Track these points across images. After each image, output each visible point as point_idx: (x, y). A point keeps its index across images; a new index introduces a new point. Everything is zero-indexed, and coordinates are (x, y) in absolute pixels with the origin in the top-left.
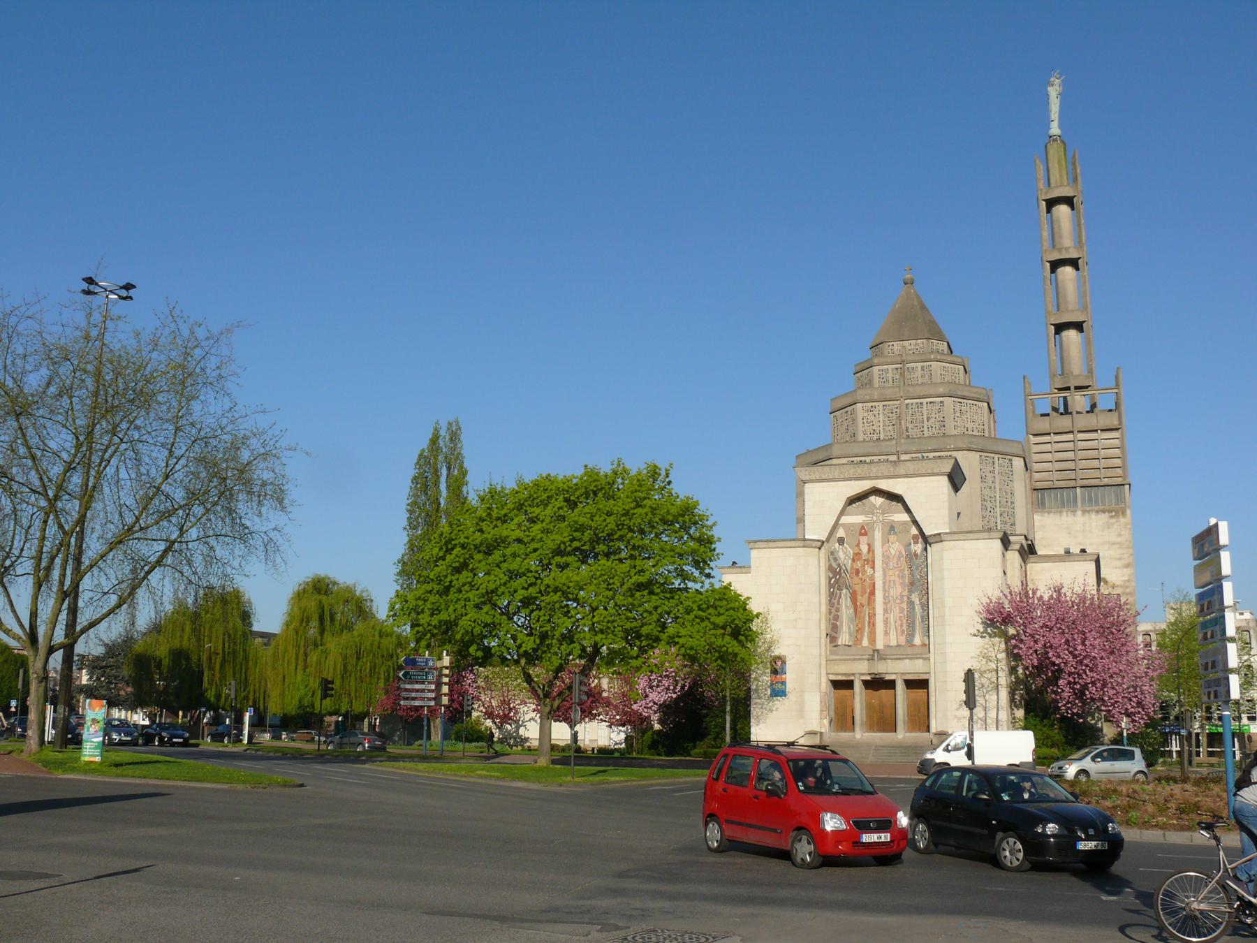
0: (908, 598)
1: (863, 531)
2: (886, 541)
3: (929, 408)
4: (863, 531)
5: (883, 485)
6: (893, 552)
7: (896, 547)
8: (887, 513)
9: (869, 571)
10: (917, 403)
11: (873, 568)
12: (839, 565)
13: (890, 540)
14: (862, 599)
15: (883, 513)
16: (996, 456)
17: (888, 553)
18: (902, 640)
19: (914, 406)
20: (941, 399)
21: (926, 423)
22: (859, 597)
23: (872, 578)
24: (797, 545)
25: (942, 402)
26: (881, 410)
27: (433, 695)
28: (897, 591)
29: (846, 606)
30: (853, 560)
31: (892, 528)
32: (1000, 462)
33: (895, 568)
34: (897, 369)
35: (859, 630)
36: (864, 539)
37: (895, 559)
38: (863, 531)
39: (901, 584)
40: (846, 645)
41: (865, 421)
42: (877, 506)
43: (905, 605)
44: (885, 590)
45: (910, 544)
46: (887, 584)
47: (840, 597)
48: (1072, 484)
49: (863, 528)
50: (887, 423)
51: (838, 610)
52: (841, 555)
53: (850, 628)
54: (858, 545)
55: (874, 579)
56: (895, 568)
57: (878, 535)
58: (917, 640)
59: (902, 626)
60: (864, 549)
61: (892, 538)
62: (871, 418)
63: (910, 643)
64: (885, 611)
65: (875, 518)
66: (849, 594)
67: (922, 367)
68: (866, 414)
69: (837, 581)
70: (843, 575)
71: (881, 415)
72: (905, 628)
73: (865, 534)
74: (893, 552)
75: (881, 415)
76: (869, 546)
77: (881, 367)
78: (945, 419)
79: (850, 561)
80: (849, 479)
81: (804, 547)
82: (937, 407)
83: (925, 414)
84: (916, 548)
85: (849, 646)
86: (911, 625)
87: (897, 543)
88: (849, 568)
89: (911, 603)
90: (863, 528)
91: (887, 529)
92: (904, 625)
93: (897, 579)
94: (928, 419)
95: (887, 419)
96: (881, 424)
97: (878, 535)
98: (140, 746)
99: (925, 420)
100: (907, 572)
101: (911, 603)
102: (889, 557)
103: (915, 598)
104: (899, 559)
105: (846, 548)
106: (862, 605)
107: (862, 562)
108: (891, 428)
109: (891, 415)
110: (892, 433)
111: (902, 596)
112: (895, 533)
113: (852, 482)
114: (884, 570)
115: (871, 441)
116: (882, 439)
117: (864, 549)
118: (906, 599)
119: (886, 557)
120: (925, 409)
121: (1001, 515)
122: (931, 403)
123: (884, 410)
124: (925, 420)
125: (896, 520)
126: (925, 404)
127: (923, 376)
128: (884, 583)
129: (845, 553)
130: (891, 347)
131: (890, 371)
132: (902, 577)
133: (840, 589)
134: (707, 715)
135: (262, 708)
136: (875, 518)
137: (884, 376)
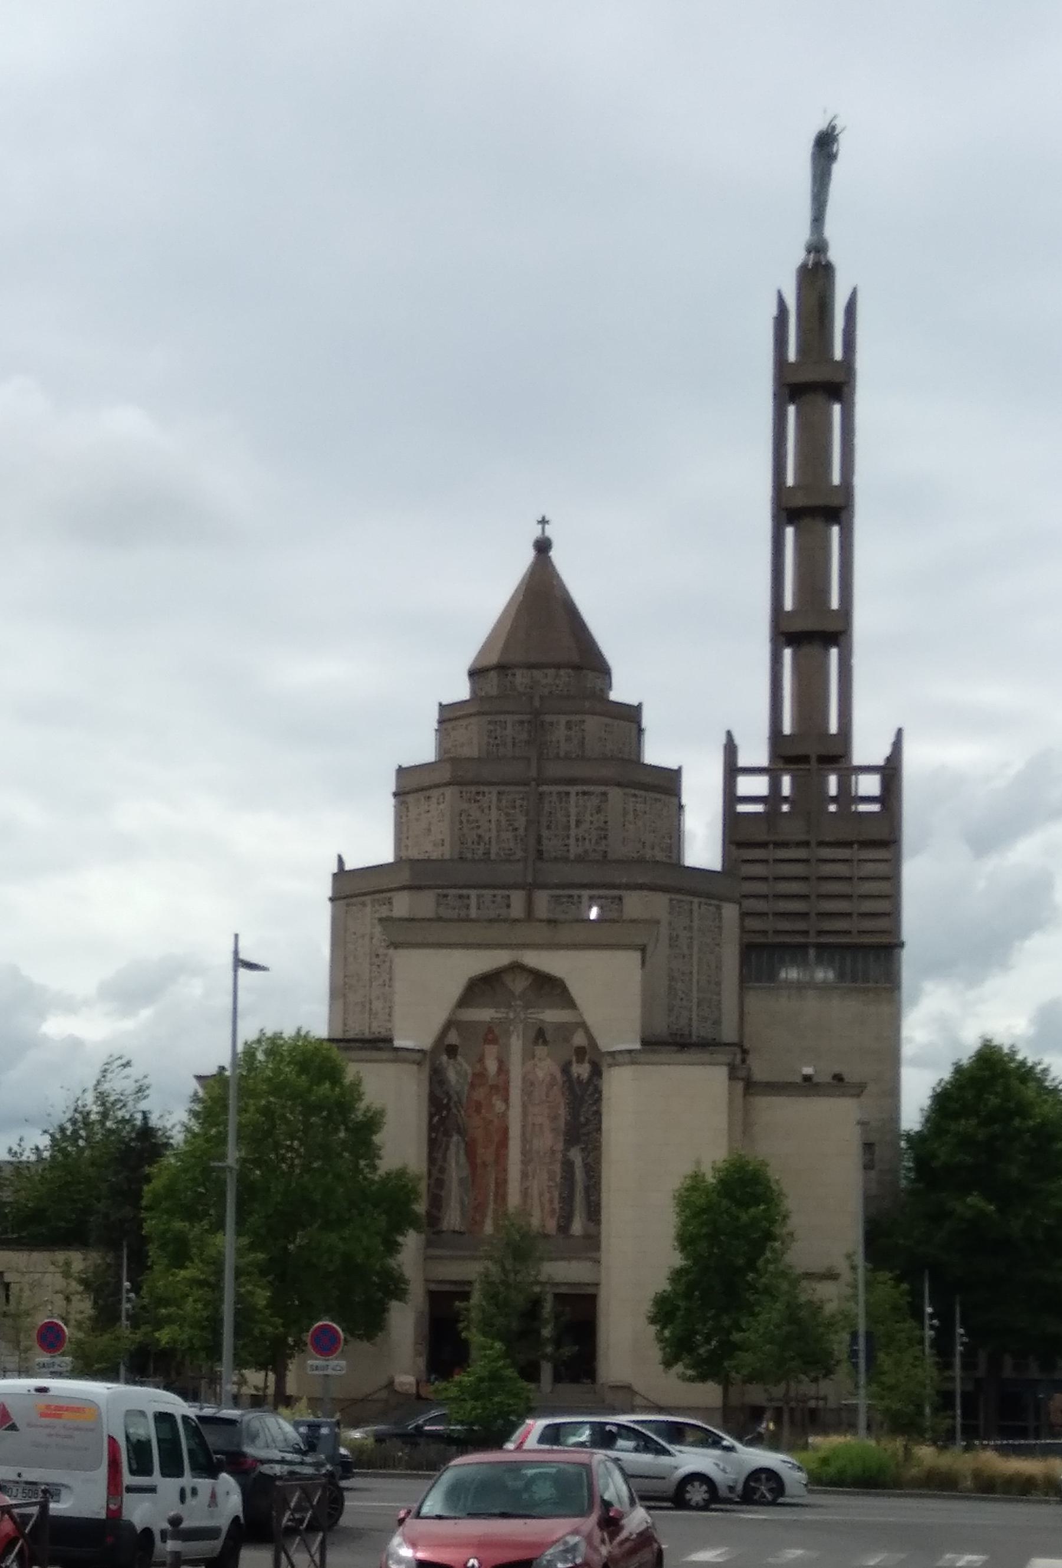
0: (564, 1156)
2: (528, 1055)
3: (581, 802)
4: (490, 1037)
5: (533, 959)
7: (546, 1067)
9: (499, 1105)
10: (559, 793)
11: (506, 1100)
12: (447, 1093)
14: (485, 1154)
15: (527, 1007)
16: (696, 900)
18: (551, 1226)
19: (554, 798)
20: (603, 789)
21: (573, 832)
22: (480, 1151)
23: (504, 1116)
25: (604, 794)
28: (547, 1141)
29: (457, 1163)
30: (472, 1085)
32: (703, 907)
34: (522, 722)
35: (480, 1208)
38: (491, 1034)
39: (553, 1130)
40: (454, 1232)
41: (464, 818)
42: (517, 994)
43: (557, 1168)
44: (524, 1140)
45: (569, 1064)
47: (447, 1148)
48: (801, 939)
49: (490, 1030)
51: (442, 1170)
52: (452, 1075)
53: (462, 1203)
54: (481, 1060)
57: (516, 1045)
58: (577, 1227)
59: (551, 1201)
60: (492, 1066)
61: (541, 1050)
63: (564, 1228)
64: (524, 1175)
65: (512, 1015)
66: (463, 1145)
67: (568, 722)
68: (465, 806)
69: (442, 1120)
70: (454, 1111)
71: (493, 807)
72: (556, 1205)
73: (494, 1041)
74: (540, 1074)
75: (493, 807)
79: (466, 1088)
80: (479, 946)
82: (595, 801)
85: (461, 1233)
86: (567, 1201)
88: (464, 1100)
89: (568, 1166)
90: (490, 1030)
91: (532, 1034)
92: (556, 1201)
94: (578, 823)
95: (503, 819)
96: (493, 826)
97: (516, 1045)
99: (573, 824)
100: (562, 1111)
101: (568, 1166)
102: (532, 1084)
103: (576, 1155)
105: (461, 1065)
106: (485, 1165)
108: (510, 835)
110: (512, 845)
111: (553, 1152)
112: (545, 1042)
114: (524, 1106)
116: (493, 856)
117: (492, 1066)
118: (559, 1156)
119: (529, 1084)
121: (699, 1005)
122: (584, 793)
123: (499, 800)
124: (573, 824)
127: (568, 739)
129: (458, 1073)
131: (509, 726)
132: (554, 1118)
133: (447, 1134)
135: (652, 1405)
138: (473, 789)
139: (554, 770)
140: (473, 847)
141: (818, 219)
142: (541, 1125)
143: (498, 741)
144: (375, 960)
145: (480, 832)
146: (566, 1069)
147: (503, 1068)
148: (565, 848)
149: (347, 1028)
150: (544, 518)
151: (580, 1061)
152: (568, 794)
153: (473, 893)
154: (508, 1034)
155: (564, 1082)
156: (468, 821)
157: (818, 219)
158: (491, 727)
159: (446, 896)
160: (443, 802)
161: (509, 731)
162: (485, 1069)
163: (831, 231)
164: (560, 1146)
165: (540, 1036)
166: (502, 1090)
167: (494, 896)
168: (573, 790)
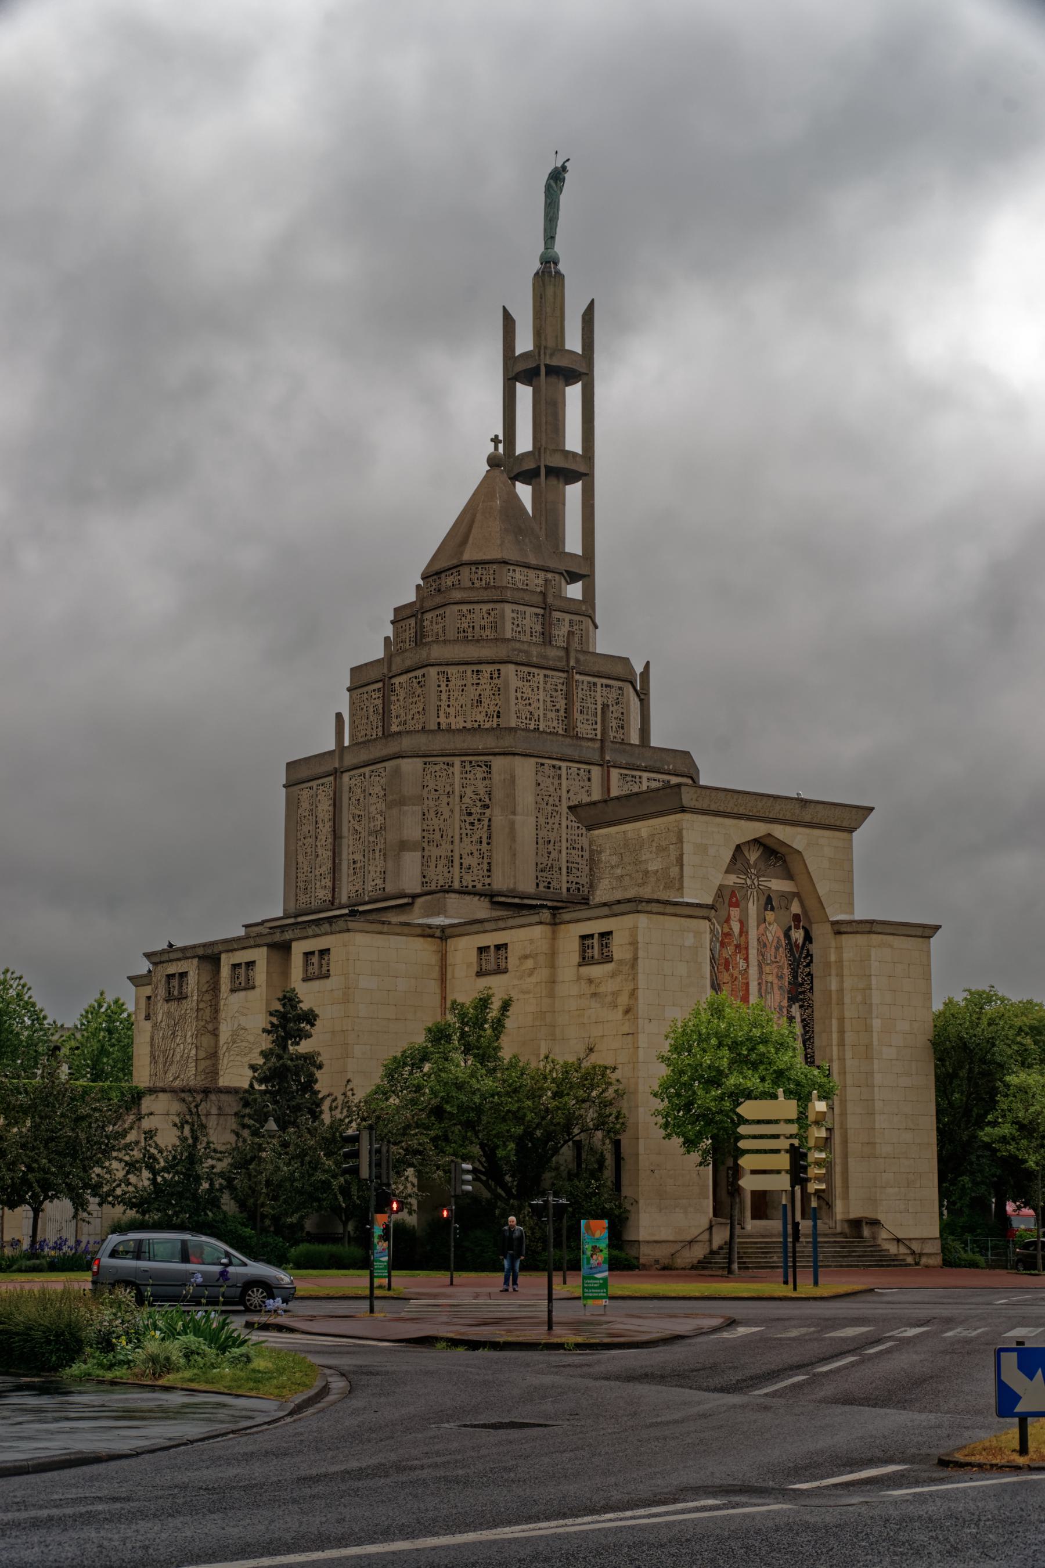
1: (734, 900)
2: (762, 920)
3: (605, 694)
5: (781, 832)
6: (770, 938)
7: (774, 932)
8: (764, 876)
10: (589, 683)
11: (746, 959)
13: (767, 918)
17: (764, 938)
24: (701, 914)
25: (620, 688)
26: (541, 683)
27: (794, 1129)
31: (769, 900)
33: (773, 962)
34: (537, 615)
36: (735, 912)
37: (773, 950)
39: (780, 988)
41: (519, 695)
42: (752, 862)
45: (790, 928)
46: (764, 987)
50: (549, 704)
54: (728, 920)
55: (747, 978)
56: (773, 962)
57: (753, 909)
61: (770, 916)
62: (528, 692)
68: (520, 684)
71: (541, 690)
73: (737, 905)
75: (541, 690)
76: (743, 923)
77: (515, 607)
78: (625, 718)
81: (611, 916)
83: (599, 703)
84: (797, 935)
87: (775, 924)
88: (717, 956)
93: (776, 981)
95: (548, 699)
98: (199, 1272)
100: (786, 971)
104: (777, 949)
107: (733, 948)
109: (554, 694)
110: (555, 724)
111: (781, 1008)
112: (772, 909)
113: (742, 822)
114: (760, 966)
115: (527, 730)
116: (541, 729)
117: (736, 927)
119: (762, 944)
120: (599, 694)
122: (607, 686)
123: (546, 683)
125: (774, 888)
126: (599, 686)
128: (759, 984)
130: (511, 574)
132: (780, 977)
134: (125, 1290)
136: (749, 882)
137: (520, 622)
138: (527, 669)
139: (437, 652)
140: (525, 722)
141: (550, 237)
142: (772, 983)
143: (519, 629)
144: (467, 818)
145: (531, 709)
146: (787, 935)
147: (744, 931)
148: (594, 732)
149: (426, 880)
150: (492, 440)
151: (797, 927)
152: (595, 684)
153: (457, 761)
154: (746, 898)
155: (787, 945)
156: (522, 697)
157: (550, 237)
158: (515, 615)
159: (542, 764)
160: (498, 677)
161: (527, 622)
162: (731, 929)
163: (560, 247)
164: (785, 1003)
165: (768, 903)
166: (742, 948)
167: (579, 769)
168: (599, 681)
